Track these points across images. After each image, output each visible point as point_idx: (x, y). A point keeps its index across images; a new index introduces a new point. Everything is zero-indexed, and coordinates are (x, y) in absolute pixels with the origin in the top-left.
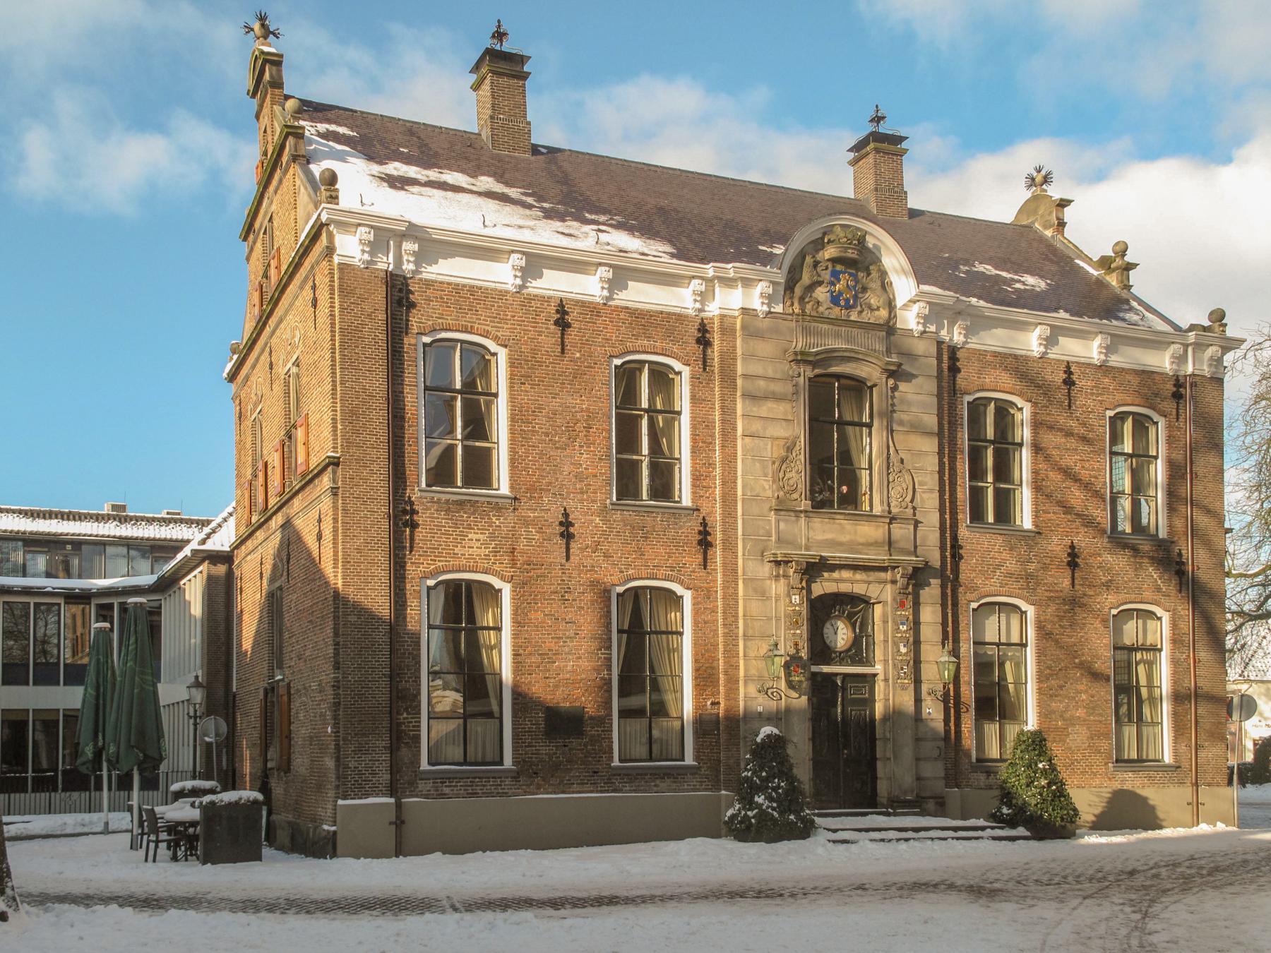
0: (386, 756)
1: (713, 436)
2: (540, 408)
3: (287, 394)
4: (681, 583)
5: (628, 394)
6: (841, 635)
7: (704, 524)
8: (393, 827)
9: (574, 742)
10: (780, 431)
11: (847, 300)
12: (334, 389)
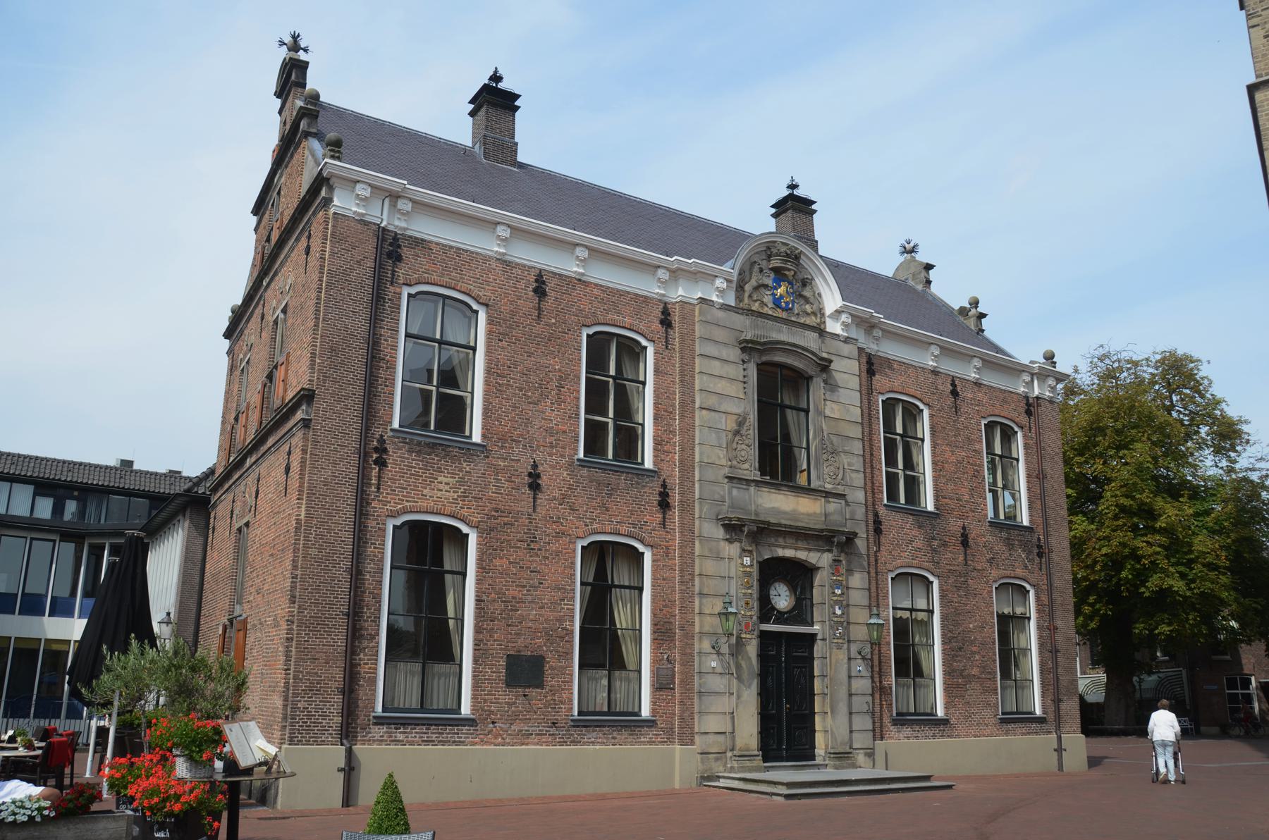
0: (338, 699)
1: (674, 406)
2: (516, 364)
3: (274, 339)
4: (642, 542)
5: (596, 361)
6: (782, 599)
7: (664, 486)
8: (342, 775)
9: (533, 692)
10: (736, 408)
11: (787, 303)
12: (316, 325)
